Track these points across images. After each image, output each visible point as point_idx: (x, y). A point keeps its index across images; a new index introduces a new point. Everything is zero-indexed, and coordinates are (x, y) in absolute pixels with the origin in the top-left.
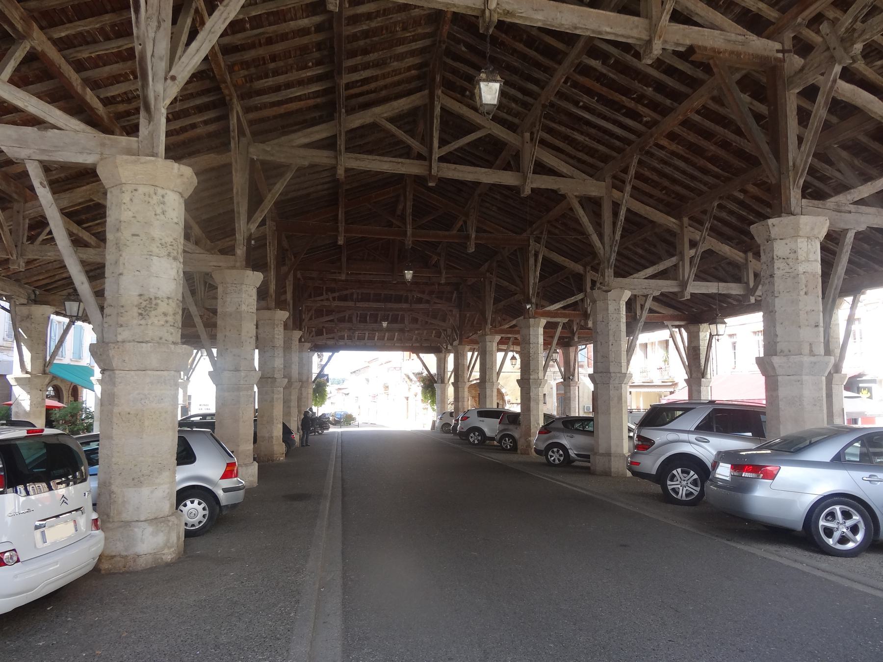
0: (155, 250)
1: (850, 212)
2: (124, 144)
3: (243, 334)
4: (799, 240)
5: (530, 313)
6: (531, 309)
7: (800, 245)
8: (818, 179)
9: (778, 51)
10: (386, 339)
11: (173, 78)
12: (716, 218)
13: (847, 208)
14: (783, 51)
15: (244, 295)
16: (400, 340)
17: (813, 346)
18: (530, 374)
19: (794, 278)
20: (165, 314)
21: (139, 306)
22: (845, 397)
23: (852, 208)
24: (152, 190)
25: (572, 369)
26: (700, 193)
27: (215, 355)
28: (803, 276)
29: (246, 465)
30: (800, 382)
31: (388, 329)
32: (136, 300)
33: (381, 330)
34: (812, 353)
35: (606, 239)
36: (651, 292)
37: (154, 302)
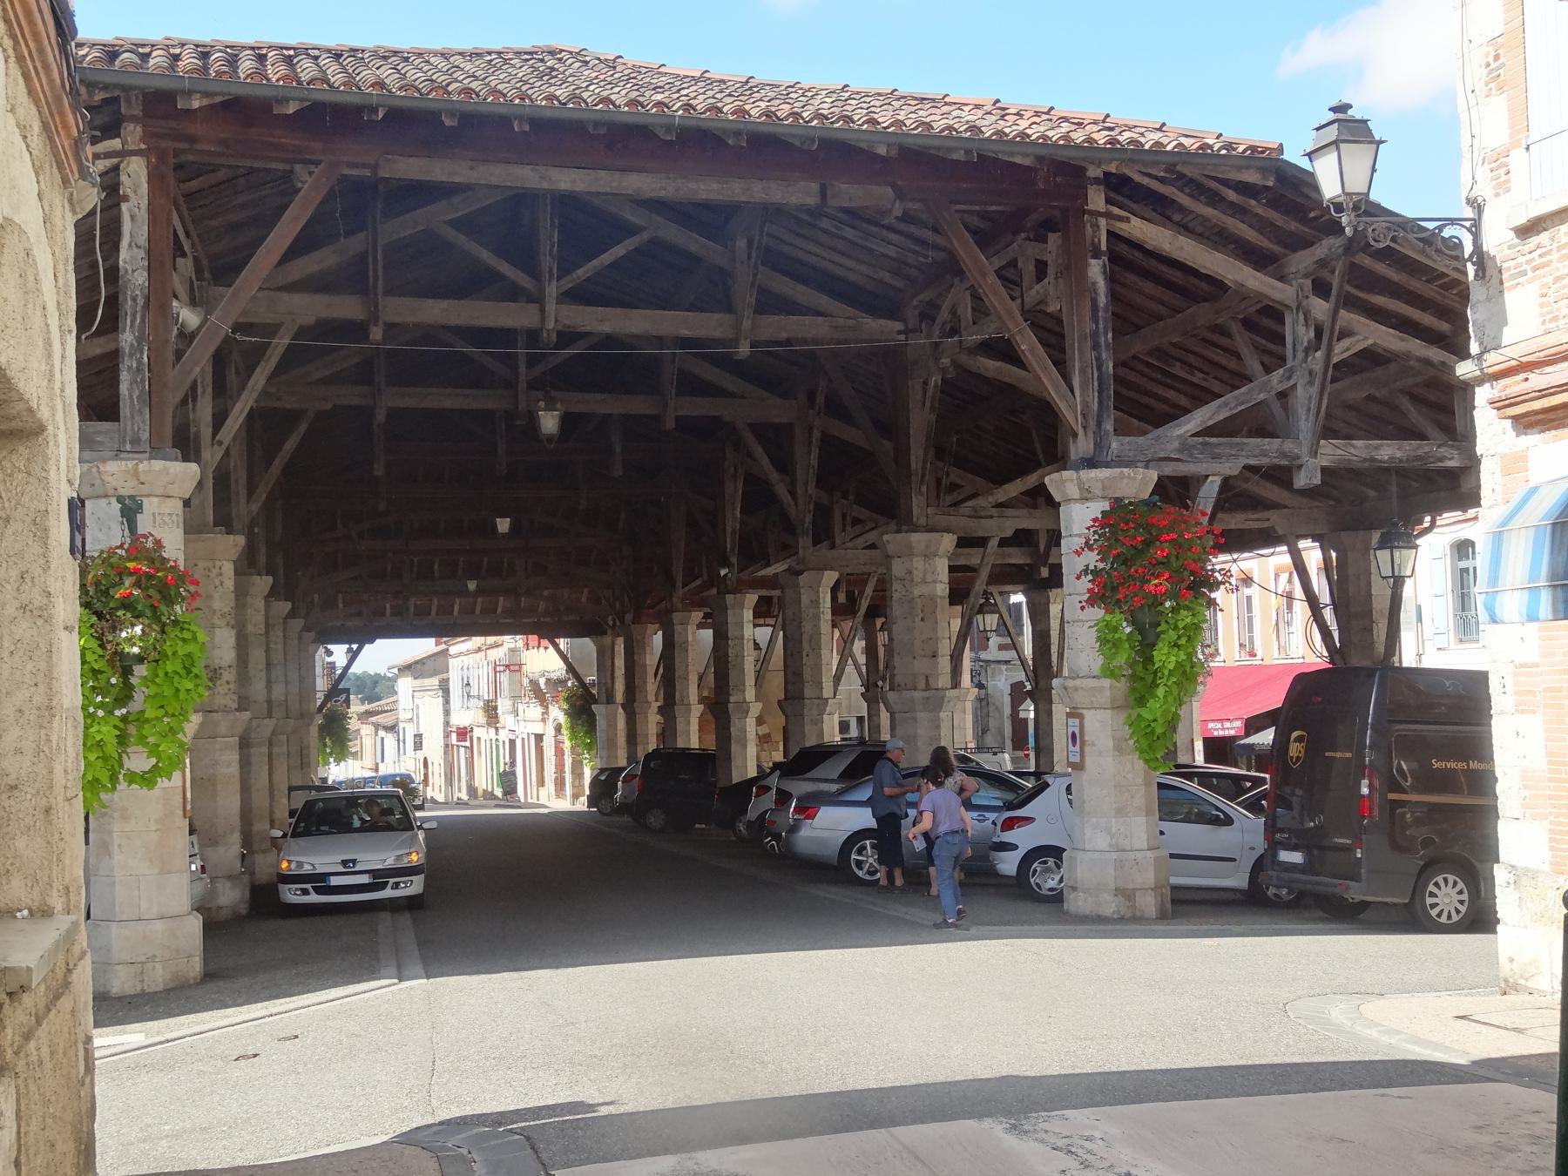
0: (217, 622)
1: (992, 517)
3: (250, 666)
4: (914, 560)
5: (728, 582)
6: (730, 575)
7: (915, 565)
9: (900, 333)
10: (478, 611)
11: (220, 443)
13: (988, 513)
14: (906, 332)
15: (249, 611)
16: (508, 612)
17: (930, 679)
18: (729, 694)
19: (910, 602)
20: (228, 683)
23: (994, 511)
28: (919, 600)
29: (264, 851)
30: (915, 719)
31: (480, 591)
33: (464, 592)
36: (874, 568)
37: (218, 672)
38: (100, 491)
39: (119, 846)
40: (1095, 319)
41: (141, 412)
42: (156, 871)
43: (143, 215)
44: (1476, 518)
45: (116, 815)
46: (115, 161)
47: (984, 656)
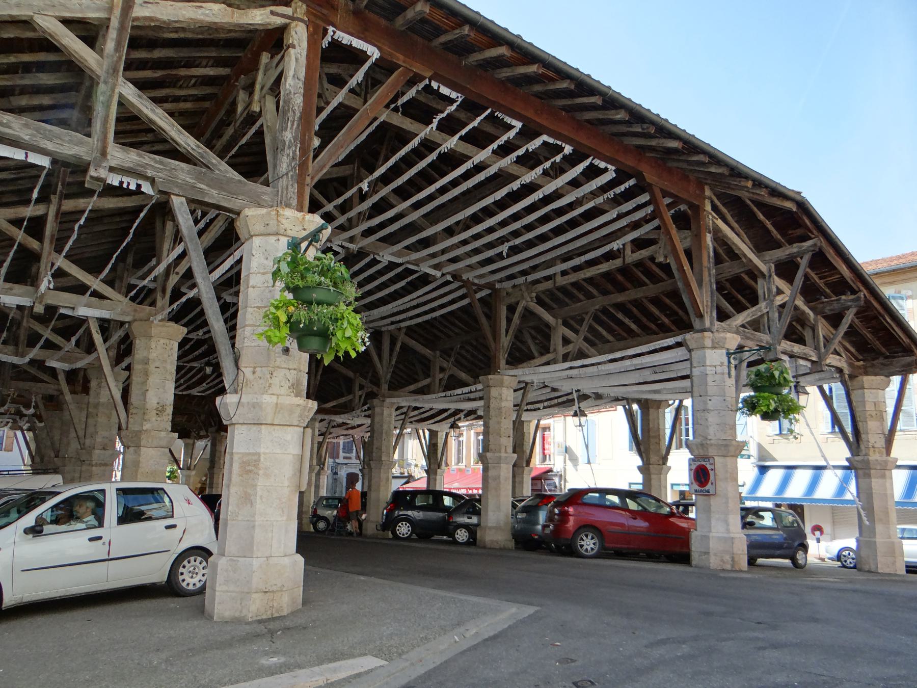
0: (168, 377)
2: (147, 311)
8: (519, 341)
12: (458, 353)
17: (778, 432)
21: (157, 409)
24: (168, 341)
25: (323, 460)
26: (449, 337)
32: (155, 406)
34: (506, 452)
35: (385, 362)
38: (273, 228)
39: (261, 497)
40: (709, 262)
41: (292, 185)
42: (285, 518)
43: (303, 60)
44: (616, 410)
45: (261, 472)
46: (288, 21)
47: (337, 461)
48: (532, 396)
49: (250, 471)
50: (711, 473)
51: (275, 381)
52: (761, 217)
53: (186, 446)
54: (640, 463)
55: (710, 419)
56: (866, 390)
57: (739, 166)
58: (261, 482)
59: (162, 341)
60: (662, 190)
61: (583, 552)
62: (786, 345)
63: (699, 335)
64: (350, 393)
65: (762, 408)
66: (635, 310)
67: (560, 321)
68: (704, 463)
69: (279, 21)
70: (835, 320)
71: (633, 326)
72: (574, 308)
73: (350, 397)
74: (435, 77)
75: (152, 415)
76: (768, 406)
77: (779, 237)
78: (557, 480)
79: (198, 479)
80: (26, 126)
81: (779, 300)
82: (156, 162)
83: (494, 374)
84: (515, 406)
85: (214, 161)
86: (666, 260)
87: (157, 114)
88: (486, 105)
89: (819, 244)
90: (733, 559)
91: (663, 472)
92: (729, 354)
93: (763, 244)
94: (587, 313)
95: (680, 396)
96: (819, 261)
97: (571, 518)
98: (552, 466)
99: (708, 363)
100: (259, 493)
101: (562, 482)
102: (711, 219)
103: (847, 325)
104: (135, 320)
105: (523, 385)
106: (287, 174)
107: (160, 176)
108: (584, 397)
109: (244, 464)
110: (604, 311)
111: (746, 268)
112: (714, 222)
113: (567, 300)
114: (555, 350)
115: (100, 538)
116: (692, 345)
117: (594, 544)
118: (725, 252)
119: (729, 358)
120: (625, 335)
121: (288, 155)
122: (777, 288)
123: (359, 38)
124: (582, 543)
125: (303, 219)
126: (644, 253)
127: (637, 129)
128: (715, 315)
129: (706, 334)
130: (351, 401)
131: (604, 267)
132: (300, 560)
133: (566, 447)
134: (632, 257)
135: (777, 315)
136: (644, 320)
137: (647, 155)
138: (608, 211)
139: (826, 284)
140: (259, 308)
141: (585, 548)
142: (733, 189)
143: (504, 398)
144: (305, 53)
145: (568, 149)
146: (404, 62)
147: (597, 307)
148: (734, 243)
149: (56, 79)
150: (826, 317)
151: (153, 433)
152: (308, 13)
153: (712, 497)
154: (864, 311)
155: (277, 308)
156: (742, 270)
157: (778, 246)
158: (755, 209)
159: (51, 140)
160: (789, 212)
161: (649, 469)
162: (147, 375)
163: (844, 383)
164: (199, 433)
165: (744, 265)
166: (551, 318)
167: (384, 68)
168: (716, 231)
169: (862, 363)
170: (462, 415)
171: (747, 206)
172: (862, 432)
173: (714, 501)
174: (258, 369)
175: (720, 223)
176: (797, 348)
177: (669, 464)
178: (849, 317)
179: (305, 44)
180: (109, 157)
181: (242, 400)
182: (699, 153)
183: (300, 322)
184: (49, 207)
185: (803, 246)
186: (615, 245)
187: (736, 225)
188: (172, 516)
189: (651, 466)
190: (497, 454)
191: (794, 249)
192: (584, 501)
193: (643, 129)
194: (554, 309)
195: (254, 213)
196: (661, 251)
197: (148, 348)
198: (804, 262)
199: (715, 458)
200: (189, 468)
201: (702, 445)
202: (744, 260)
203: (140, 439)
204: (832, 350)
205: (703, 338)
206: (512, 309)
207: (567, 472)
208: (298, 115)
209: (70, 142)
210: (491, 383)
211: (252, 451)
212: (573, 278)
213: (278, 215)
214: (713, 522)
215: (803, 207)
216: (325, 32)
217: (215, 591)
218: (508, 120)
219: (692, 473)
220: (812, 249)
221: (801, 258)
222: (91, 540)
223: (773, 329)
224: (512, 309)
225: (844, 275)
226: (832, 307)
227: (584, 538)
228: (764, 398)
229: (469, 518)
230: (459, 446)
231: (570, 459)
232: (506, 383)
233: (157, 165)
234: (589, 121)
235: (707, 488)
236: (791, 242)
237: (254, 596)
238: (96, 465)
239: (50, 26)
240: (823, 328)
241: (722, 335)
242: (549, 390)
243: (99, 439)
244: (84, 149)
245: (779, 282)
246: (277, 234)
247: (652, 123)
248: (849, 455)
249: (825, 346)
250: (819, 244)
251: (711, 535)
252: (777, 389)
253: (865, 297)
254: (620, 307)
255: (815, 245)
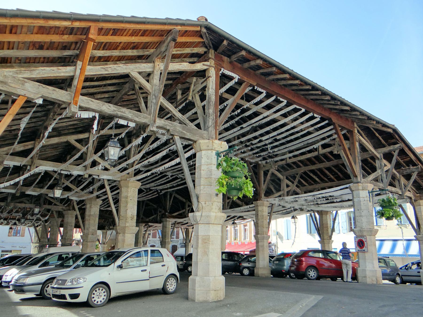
21: (131, 217)
22: (128, 122)
27: (62, 232)
32: (130, 216)
38: (210, 147)
39: (211, 253)
45: (210, 243)
48: (275, 209)
49: (206, 242)
50: (365, 243)
51: (214, 207)
52: (377, 135)
53: (103, 233)
54: (319, 239)
55: (363, 220)
56: (421, 206)
57: (372, 116)
58: (211, 247)
59: (133, 189)
60: (338, 125)
61: (310, 277)
62: (390, 188)
63: (356, 184)
64: (183, 209)
65: (387, 215)
66: (318, 172)
67: (285, 177)
68: (362, 239)
69: (205, 67)
70: (408, 177)
71: (317, 179)
72: (291, 172)
73: (184, 210)
74: (258, 85)
75: (129, 220)
76: (389, 214)
77: (384, 143)
78: (273, 247)
79: (107, 249)
80: (130, 112)
81: (386, 169)
82: (170, 123)
83: (259, 201)
84: (268, 213)
85: (188, 122)
86: (338, 153)
87: (169, 105)
88: (273, 94)
89: (402, 146)
90: (377, 280)
91: (330, 243)
92: (369, 192)
93: (378, 145)
94: (297, 174)
95: (336, 209)
96: (402, 152)
97: (304, 263)
98: (271, 241)
99: (361, 196)
100: (210, 251)
101: (276, 248)
102: (357, 136)
103: (414, 179)
104: (122, 180)
105: (271, 205)
106: (211, 126)
107: (171, 129)
108: (295, 210)
109: (203, 240)
110: (305, 173)
111: (370, 156)
112: (358, 137)
113: (288, 168)
114: (283, 190)
115: (146, 270)
116: (353, 188)
117: (314, 274)
118: (363, 149)
119: (369, 194)
120: (313, 183)
121: (211, 118)
122: (385, 164)
123: (232, 72)
124: (310, 273)
125: (221, 143)
126: (328, 150)
127: (333, 102)
128: (362, 176)
129: (359, 184)
130: (184, 212)
131: (309, 156)
132: (223, 278)
133: (277, 232)
134: (322, 151)
135: (385, 175)
136: (322, 176)
137: (333, 111)
138: (313, 133)
139: (404, 162)
140: (206, 178)
141: (311, 275)
142: (366, 124)
143: (264, 211)
144: (215, 79)
145: (303, 110)
146: (247, 80)
147: (302, 171)
148: (366, 146)
149: (114, 88)
150: (404, 176)
151: (130, 227)
152: (215, 64)
153: (366, 253)
154: (420, 173)
155: (222, 179)
156: (368, 156)
157: (384, 146)
158: (375, 132)
159: (137, 117)
160: (390, 133)
161: (324, 242)
162: (127, 203)
163: (412, 203)
164: (109, 227)
165: (369, 154)
166: (281, 176)
167: (240, 83)
168: (360, 141)
169: (418, 195)
170: (236, 218)
171: (372, 130)
172: (421, 224)
173: (366, 254)
174: (207, 202)
175: (361, 137)
176: (393, 189)
177: (332, 239)
178: (414, 176)
179: (214, 76)
180: (156, 123)
181: (202, 215)
182: (356, 111)
183: (232, 185)
184: (90, 134)
185: (395, 147)
186: (315, 146)
187: (366, 138)
188: (163, 261)
189: (325, 240)
190: (263, 236)
191: (391, 148)
192: (309, 255)
193: (335, 103)
194: (282, 172)
195: (203, 142)
196: (336, 149)
197: (127, 192)
198: (396, 154)
199: (367, 236)
200: (104, 244)
201: (361, 231)
202: (370, 152)
203: (125, 230)
204: (407, 190)
205: (358, 186)
206: (266, 174)
207: (278, 243)
208: (214, 103)
209: (143, 117)
210: (259, 204)
211: (206, 234)
212: (294, 160)
213: (213, 142)
214: (367, 264)
215: (395, 131)
216: (221, 70)
217: (195, 290)
218: (281, 99)
219: (356, 242)
220: (399, 148)
221: (394, 152)
222: (142, 271)
223: (383, 181)
224: (266, 174)
225: (412, 159)
226: (407, 172)
227: (310, 271)
228: (387, 211)
229: (248, 264)
230: (235, 231)
231: (279, 238)
232: (265, 204)
233: (170, 125)
234: (312, 99)
235: (364, 249)
236: (390, 145)
237: (211, 292)
238: (89, 242)
239: (135, 75)
240: (403, 181)
241: (366, 184)
242: (281, 207)
243: (90, 230)
244: (147, 120)
245: (385, 162)
246: (212, 150)
247: (339, 100)
248: (415, 234)
249: (404, 188)
250: (402, 146)
251: (367, 269)
252: (392, 207)
253: (421, 167)
254: (312, 171)
255: (400, 146)
